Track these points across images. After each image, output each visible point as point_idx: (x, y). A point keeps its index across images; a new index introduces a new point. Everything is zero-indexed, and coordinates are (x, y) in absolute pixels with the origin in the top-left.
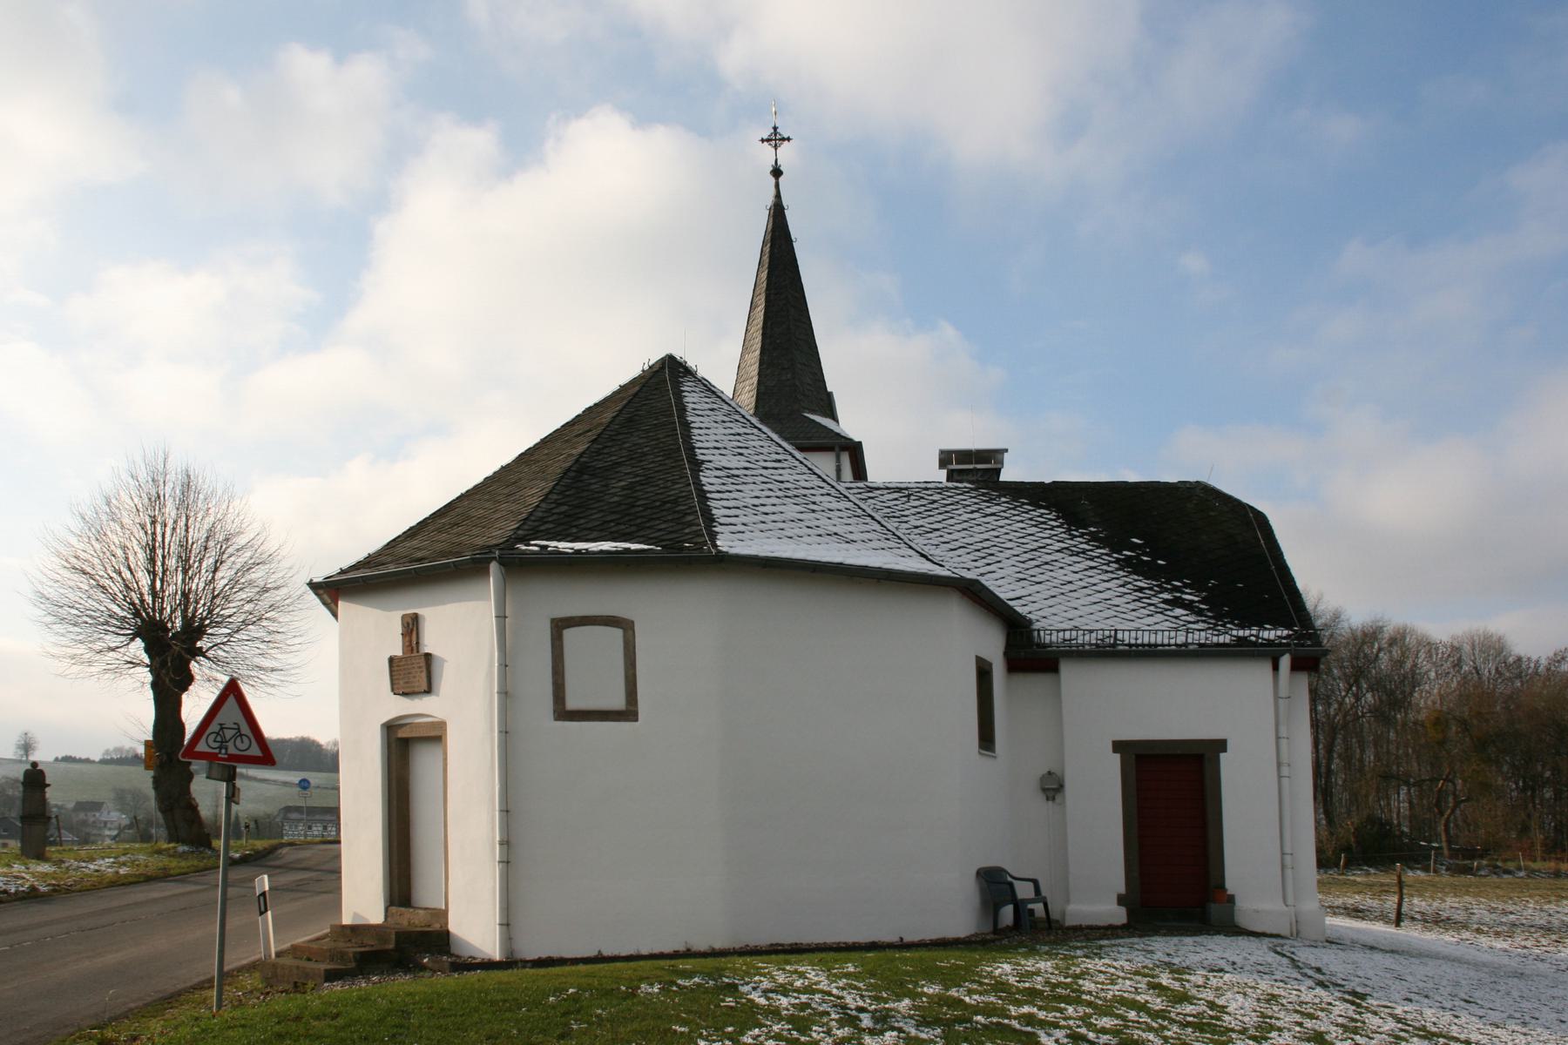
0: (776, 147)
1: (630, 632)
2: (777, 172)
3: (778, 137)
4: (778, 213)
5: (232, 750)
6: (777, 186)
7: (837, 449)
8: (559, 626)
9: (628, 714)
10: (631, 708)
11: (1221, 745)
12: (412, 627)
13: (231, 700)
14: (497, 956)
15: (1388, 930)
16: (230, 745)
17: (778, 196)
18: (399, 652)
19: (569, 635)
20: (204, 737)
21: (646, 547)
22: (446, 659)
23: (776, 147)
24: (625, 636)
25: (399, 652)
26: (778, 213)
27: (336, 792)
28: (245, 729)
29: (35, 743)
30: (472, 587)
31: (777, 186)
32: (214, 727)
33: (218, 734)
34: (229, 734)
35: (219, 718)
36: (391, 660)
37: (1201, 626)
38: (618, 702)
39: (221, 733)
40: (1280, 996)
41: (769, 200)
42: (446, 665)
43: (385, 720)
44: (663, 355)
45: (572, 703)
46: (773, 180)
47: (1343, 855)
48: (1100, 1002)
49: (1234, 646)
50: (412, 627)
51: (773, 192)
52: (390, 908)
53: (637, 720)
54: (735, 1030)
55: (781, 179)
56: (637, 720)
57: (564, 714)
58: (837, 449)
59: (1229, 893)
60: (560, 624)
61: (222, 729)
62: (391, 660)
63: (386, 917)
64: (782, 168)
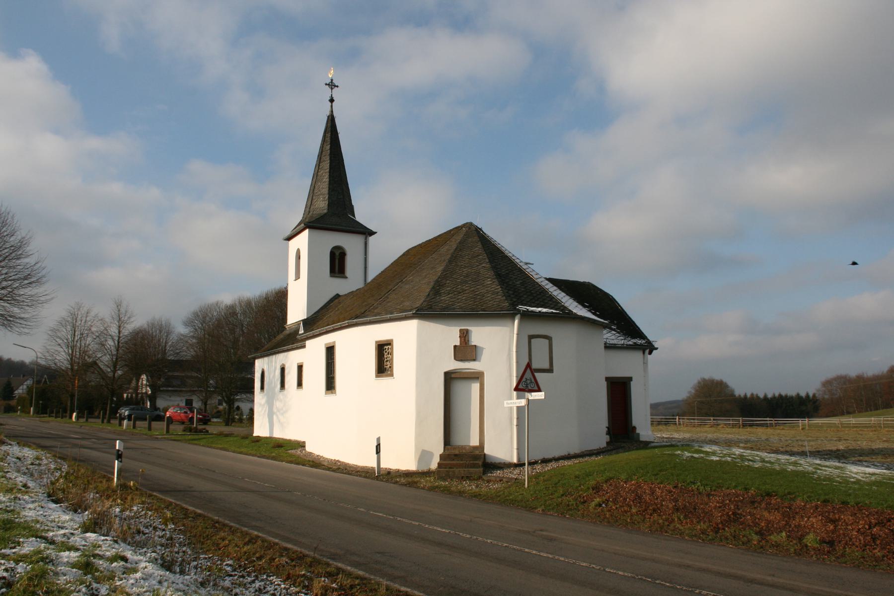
0: (332, 89)
2: (332, 100)
3: (331, 84)
4: (331, 120)
5: (530, 388)
6: (332, 106)
7: (367, 234)
8: (531, 337)
11: (630, 379)
12: (465, 335)
14: (515, 461)
16: (529, 386)
17: (332, 111)
18: (458, 344)
19: (533, 341)
20: (521, 384)
21: (554, 311)
22: (484, 347)
23: (332, 89)
24: (549, 342)
25: (458, 344)
26: (331, 120)
28: (533, 380)
30: (508, 322)
31: (332, 106)
32: (524, 379)
34: (528, 382)
35: (525, 377)
37: (622, 338)
41: (328, 113)
42: (484, 351)
43: (447, 370)
44: (469, 222)
46: (330, 104)
47: (86, 412)
48: (684, 462)
49: (634, 345)
50: (465, 335)
51: (330, 108)
52: (447, 447)
53: (553, 373)
55: (334, 103)
56: (553, 373)
58: (367, 234)
59: (633, 425)
61: (526, 380)
62: (455, 347)
63: (444, 451)
64: (334, 99)
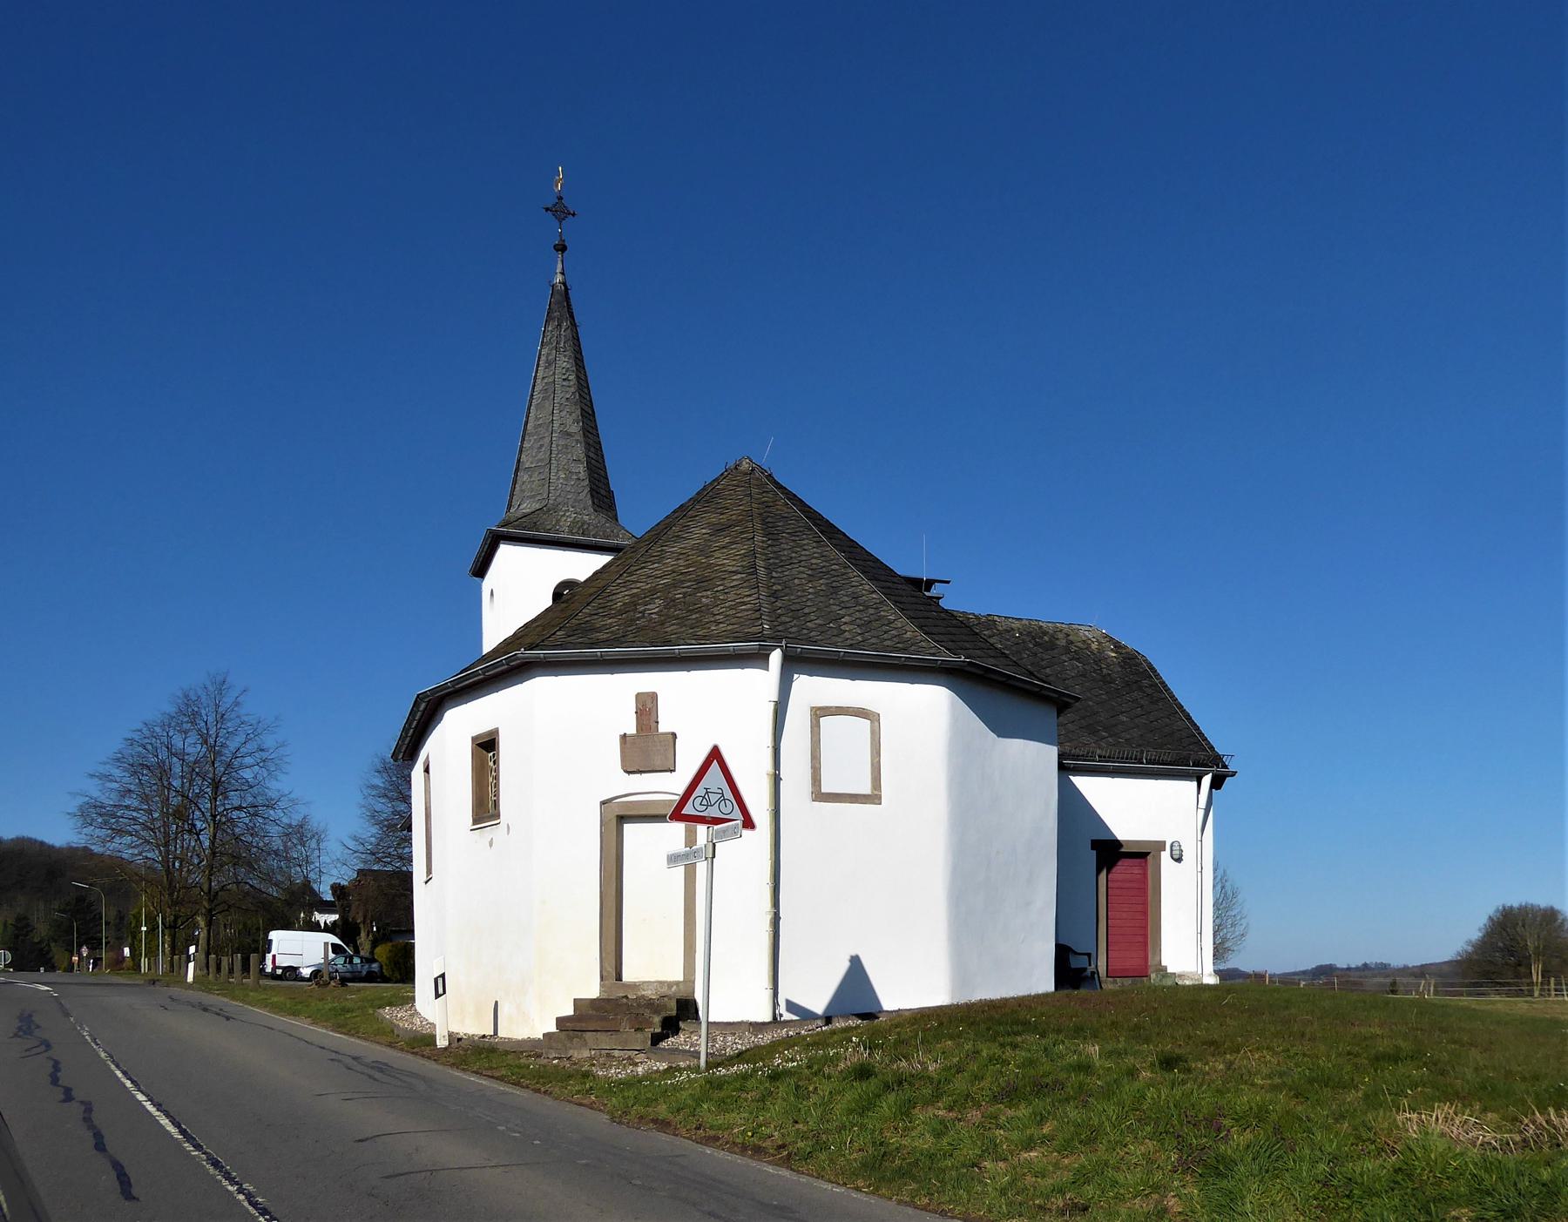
1: (877, 724)
9: (874, 798)
10: (876, 793)
13: (715, 764)
15: (492, 1085)
19: (825, 722)
27: (402, 807)
28: (729, 794)
29: (1498, 909)
32: (699, 791)
33: (704, 797)
34: (714, 798)
36: (624, 737)
38: (866, 789)
39: (706, 796)
40: (225, 886)
45: (826, 788)
54: (124, 958)
57: (820, 796)
60: (818, 712)
61: (707, 792)
62: (624, 737)
